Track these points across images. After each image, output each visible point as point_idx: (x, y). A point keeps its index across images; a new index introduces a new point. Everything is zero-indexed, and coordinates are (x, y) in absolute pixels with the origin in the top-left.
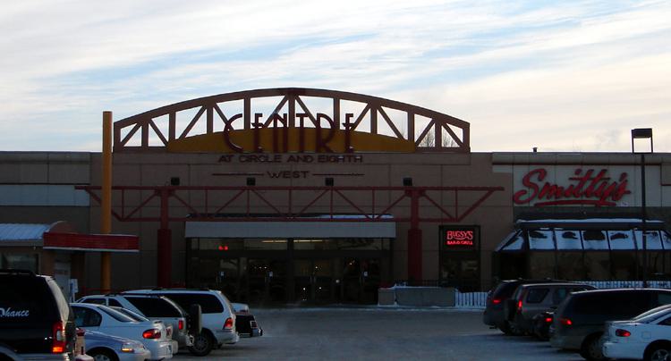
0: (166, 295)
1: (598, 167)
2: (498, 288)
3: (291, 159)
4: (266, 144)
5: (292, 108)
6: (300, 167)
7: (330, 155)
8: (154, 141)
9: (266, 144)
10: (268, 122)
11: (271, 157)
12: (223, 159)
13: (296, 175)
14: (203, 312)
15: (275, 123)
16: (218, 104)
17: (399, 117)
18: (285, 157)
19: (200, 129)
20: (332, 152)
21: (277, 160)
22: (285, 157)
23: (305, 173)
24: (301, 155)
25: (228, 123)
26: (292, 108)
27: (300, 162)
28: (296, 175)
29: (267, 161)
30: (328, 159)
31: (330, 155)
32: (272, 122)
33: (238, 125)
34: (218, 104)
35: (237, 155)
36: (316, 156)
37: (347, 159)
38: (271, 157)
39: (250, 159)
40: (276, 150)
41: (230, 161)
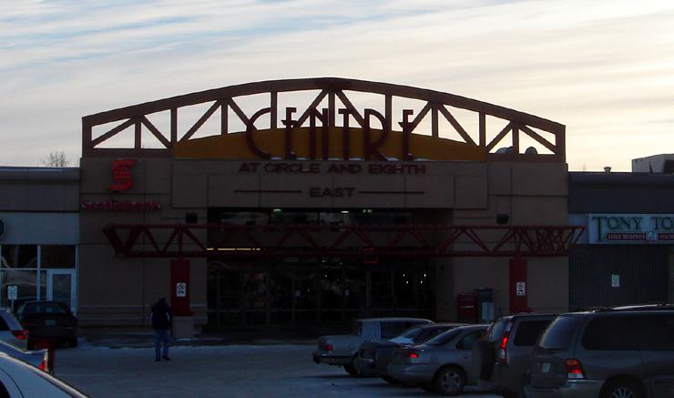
6: (346, 180)
7: (383, 163)
8: (149, 142)
10: (303, 119)
12: (244, 168)
14: (511, 261)
15: (313, 122)
17: (469, 120)
18: (324, 166)
19: (212, 128)
21: (314, 170)
22: (324, 166)
23: (350, 190)
25: (249, 123)
31: (383, 163)
33: (263, 123)
35: (264, 163)
36: (365, 165)
37: (406, 169)
39: (278, 168)
41: (255, 171)
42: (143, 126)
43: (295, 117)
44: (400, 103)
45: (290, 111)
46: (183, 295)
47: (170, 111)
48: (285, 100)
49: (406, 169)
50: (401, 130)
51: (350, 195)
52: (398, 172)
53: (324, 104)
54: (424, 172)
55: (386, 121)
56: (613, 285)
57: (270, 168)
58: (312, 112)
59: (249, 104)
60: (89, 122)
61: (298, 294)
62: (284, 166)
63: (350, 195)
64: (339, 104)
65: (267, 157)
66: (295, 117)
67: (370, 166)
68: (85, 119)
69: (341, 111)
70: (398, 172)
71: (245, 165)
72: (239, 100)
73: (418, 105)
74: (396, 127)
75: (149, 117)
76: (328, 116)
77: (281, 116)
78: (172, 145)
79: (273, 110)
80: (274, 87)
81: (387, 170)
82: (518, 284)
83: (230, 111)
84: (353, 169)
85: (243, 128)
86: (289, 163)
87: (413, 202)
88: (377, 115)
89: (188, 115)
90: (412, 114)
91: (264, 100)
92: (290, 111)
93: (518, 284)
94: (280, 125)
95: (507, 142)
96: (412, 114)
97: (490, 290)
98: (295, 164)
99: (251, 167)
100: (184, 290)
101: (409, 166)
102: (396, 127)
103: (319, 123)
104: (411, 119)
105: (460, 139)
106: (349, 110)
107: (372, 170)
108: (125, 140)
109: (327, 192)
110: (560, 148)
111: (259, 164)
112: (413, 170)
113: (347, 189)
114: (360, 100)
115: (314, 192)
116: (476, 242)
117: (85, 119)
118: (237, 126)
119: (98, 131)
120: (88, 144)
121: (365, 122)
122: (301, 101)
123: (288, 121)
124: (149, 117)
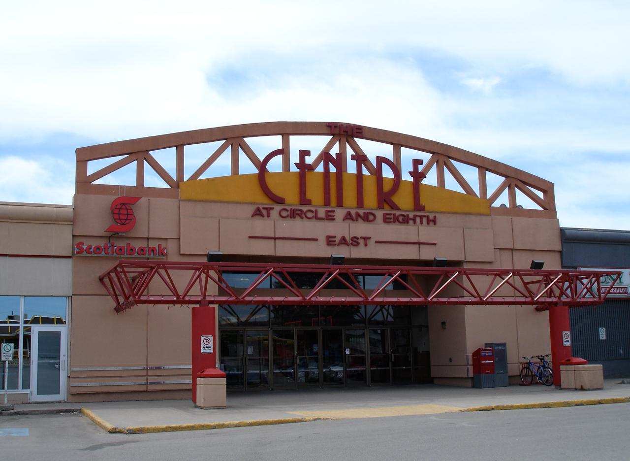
0: (247, 295)
1: (518, 293)
2: (52, 361)
3: (348, 217)
4: (315, 193)
5: (343, 149)
6: (360, 229)
7: (397, 213)
8: (153, 180)
9: (315, 193)
10: (317, 162)
11: (322, 213)
12: (258, 213)
13: (355, 241)
14: (193, 309)
15: (326, 167)
16: (247, 140)
17: (470, 174)
18: (340, 213)
19: (222, 166)
20: (397, 208)
21: (329, 217)
22: (340, 213)
23: (366, 239)
24: (361, 212)
25: (262, 166)
26: (343, 149)
27: (360, 220)
28: (355, 241)
29: (317, 218)
30: (396, 220)
31: (397, 213)
32: (322, 164)
33: (275, 165)
34: (247, 140)
35: (278, 208)
36: (379, 214)
37: (418, 220)
38: (322, 213)
39: (294, 214)
40: (327, 203)
41: (268, 216)
42: (146, 164)
43: (309, 160)
44: (408, 155)
45: (304, 154)
46: (210, 351)
47: (306, 157)
48: (298, 143)
49: (418, 220)
50: (411, 179)
51: (366, 245)
52: (411, 222)
53: (335, 151)
54: (435, 224)
55: (396, 168)
56: (601, 338)
57: (284, 214)
58: (325, 156)
59: (263, 145)
60: (85, 155)
61: (348, 352)
62: (298, 212)
63: (366, 245)
64: (350, 152)
65: (279, 201)
66: (309, 160)
67: (385, 215)
68: (79, 151)
69: (353, 158)
70: (411, 222)
71: (258, 209)
72: (250, 141)
73: (426, 157)
74: (406, 177)
75: (154, 154)
76: (340, 161)
77: (295, 158)
78: (176, 185)
79: (284, 152)
80: (286, 130)
81: (401, 219)
82: (203, 338)
83: (242, 155)
84: (367, 218)
85: (255, 171)
86: (305, 208)
87: (427, 254)
88: (387, 161)
89: (196, 155)
90: (422, 164)
91: (275, 142)
92: (304, 154)
93: (203, 338)
94: (294, 169)
95: (504, 199)
96: (422, 164)
97: (504, 345)
98: (310, 211)
99: (264, 212)
100: (211, 345)
101: (421, 217)
102: (406, 177)
103: (333, 169)
104: (421, 168)
105: (460, 190)
106: (360, 158)
107: (386, 220)
108: (125, 177)
109: (344, 241)
110: (549, 207)
111: (272, 209)
112: (425, 220)
113: (361, 238)
114: (372, 149)
115: (330, 241)
116: (147, 285)
117: (79, 151)
118: (247, 167)
119: (93, 167)
120: (84, 183)
121: (378, 172)
122: (316, 144)
123: (302, 165)
124: (154, 154)
